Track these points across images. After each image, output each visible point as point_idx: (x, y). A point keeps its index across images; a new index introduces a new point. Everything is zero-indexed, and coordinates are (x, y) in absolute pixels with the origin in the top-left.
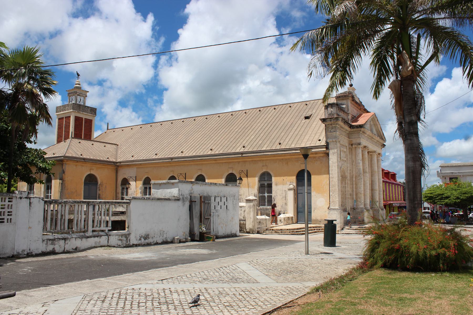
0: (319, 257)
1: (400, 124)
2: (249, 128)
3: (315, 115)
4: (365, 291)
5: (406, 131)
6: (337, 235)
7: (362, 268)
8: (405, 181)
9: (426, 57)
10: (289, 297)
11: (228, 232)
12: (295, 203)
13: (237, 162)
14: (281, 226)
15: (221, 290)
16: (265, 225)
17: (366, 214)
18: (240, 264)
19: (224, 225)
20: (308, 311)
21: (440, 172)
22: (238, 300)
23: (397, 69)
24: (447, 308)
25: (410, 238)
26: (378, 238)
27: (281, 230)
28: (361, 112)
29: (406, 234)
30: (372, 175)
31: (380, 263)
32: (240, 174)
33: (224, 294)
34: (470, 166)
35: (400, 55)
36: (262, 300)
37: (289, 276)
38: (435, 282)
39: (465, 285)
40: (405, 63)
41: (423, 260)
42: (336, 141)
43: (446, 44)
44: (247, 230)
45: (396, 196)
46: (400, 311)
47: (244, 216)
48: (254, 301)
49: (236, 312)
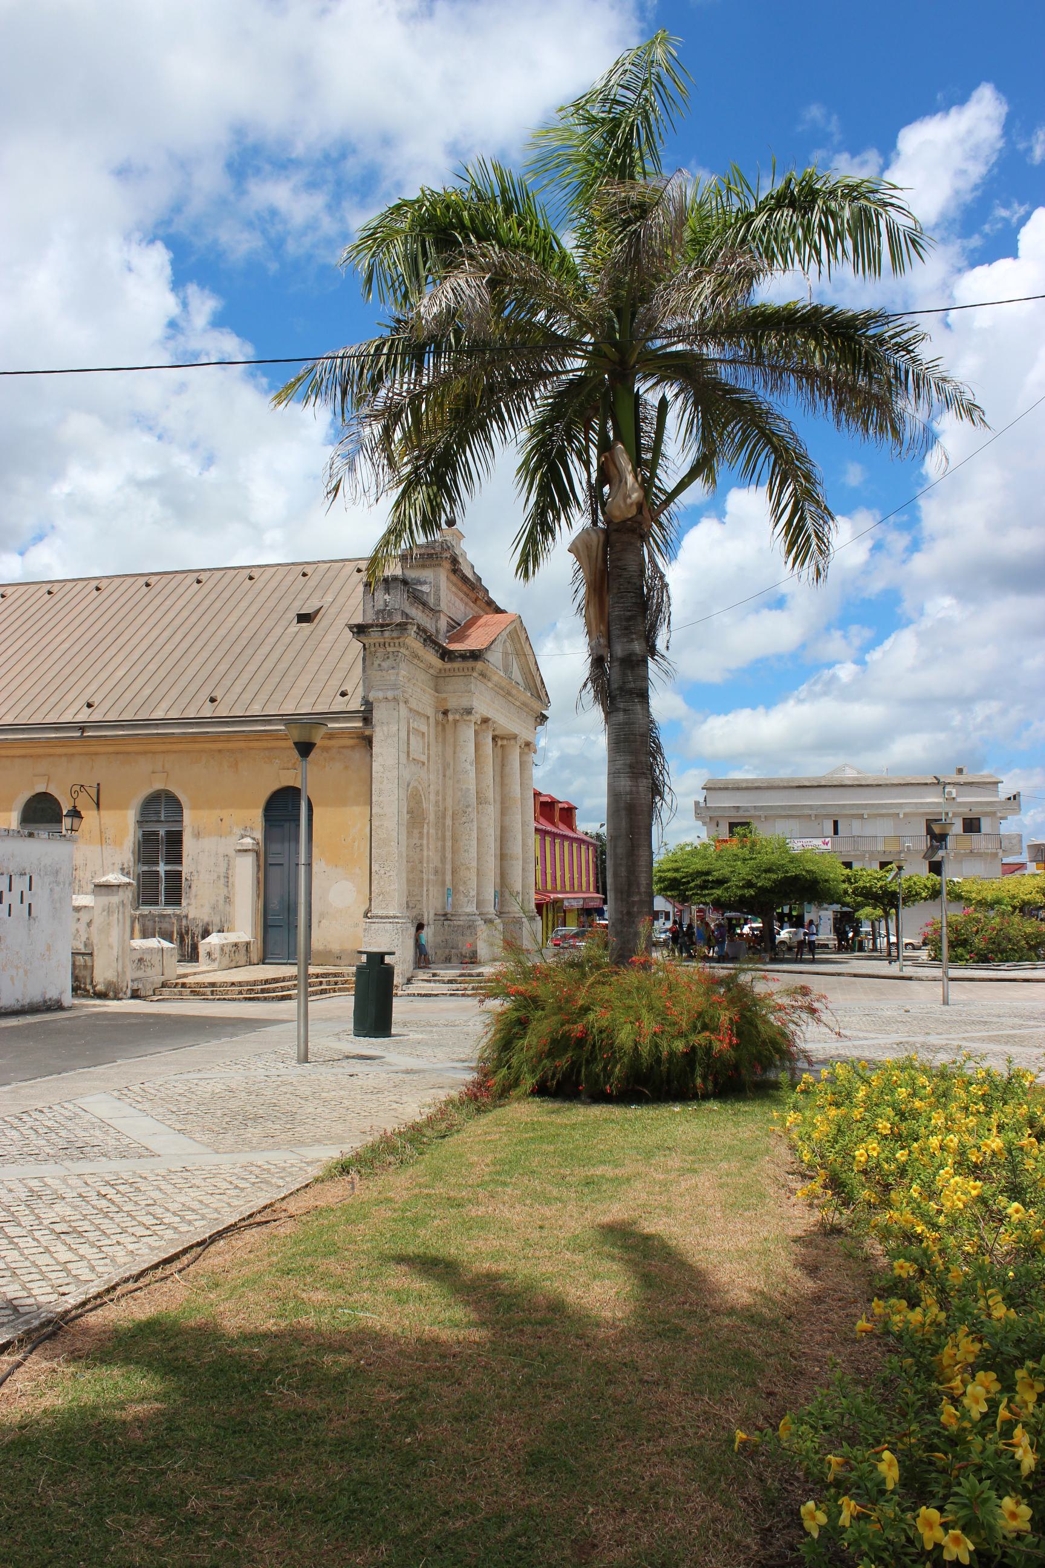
0: (341, 1070)
1: (598, 662)
2: (109, 640)
3: (333, 611)
4: (487, 1165)
5: (615, 686)
6: (395, 1000)
7: (476, 1098)
8: (604, 830)
9: (678, 464)
10: (259, 1194)
11: (33, 994)
12: (258, 896)
13: (66, 755)
14: (203, 972)
15: (34, 1184)
16: (158, 969)
17: (483, 930)
18: (89, 1099)
19: (21, 971)
20: (321, 1232)
21: (702, 805)
22: (96, 1212)
23: (595, 497)
24: (709, 1198)
25: (617, 1003)
26: (525, 1007)
27: (213, 985)
28: (477, 609)
29: (605, 992)
30: (504, 811)
31: (529, 1082)
32: (75, 796)
33: (49, 1197)
34: (785, 788)
35: (607, 454)
36: (174, 1206)
37: (253, 1132)
38: (681, 1129)
39: (758, 1132)
40: (621, 481)
41: (652, 1067)
42: (395, 699)
43: (735, 431)
44: (98, 988)
45: (572, 878)
46: (588, 1215)
47: (88, 939)
48: (151, 1214)
49: (95, 1250)
